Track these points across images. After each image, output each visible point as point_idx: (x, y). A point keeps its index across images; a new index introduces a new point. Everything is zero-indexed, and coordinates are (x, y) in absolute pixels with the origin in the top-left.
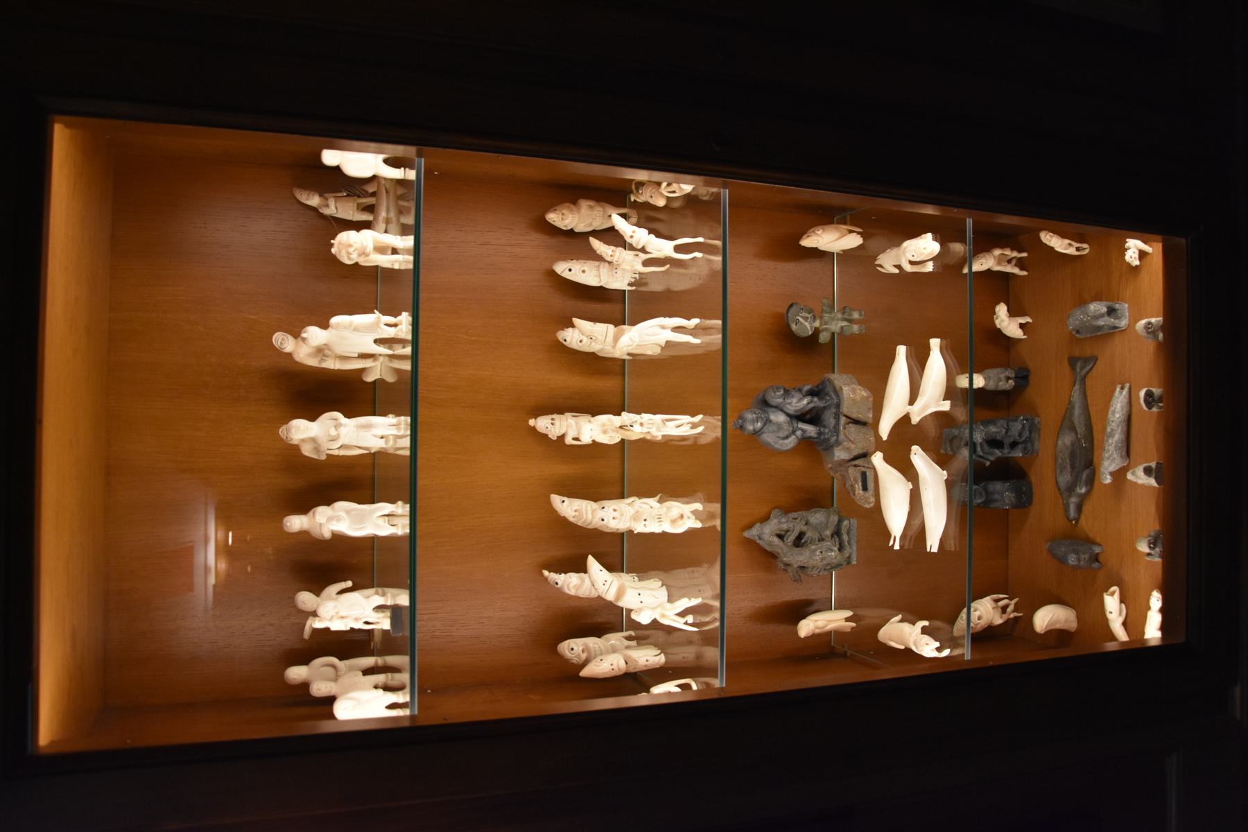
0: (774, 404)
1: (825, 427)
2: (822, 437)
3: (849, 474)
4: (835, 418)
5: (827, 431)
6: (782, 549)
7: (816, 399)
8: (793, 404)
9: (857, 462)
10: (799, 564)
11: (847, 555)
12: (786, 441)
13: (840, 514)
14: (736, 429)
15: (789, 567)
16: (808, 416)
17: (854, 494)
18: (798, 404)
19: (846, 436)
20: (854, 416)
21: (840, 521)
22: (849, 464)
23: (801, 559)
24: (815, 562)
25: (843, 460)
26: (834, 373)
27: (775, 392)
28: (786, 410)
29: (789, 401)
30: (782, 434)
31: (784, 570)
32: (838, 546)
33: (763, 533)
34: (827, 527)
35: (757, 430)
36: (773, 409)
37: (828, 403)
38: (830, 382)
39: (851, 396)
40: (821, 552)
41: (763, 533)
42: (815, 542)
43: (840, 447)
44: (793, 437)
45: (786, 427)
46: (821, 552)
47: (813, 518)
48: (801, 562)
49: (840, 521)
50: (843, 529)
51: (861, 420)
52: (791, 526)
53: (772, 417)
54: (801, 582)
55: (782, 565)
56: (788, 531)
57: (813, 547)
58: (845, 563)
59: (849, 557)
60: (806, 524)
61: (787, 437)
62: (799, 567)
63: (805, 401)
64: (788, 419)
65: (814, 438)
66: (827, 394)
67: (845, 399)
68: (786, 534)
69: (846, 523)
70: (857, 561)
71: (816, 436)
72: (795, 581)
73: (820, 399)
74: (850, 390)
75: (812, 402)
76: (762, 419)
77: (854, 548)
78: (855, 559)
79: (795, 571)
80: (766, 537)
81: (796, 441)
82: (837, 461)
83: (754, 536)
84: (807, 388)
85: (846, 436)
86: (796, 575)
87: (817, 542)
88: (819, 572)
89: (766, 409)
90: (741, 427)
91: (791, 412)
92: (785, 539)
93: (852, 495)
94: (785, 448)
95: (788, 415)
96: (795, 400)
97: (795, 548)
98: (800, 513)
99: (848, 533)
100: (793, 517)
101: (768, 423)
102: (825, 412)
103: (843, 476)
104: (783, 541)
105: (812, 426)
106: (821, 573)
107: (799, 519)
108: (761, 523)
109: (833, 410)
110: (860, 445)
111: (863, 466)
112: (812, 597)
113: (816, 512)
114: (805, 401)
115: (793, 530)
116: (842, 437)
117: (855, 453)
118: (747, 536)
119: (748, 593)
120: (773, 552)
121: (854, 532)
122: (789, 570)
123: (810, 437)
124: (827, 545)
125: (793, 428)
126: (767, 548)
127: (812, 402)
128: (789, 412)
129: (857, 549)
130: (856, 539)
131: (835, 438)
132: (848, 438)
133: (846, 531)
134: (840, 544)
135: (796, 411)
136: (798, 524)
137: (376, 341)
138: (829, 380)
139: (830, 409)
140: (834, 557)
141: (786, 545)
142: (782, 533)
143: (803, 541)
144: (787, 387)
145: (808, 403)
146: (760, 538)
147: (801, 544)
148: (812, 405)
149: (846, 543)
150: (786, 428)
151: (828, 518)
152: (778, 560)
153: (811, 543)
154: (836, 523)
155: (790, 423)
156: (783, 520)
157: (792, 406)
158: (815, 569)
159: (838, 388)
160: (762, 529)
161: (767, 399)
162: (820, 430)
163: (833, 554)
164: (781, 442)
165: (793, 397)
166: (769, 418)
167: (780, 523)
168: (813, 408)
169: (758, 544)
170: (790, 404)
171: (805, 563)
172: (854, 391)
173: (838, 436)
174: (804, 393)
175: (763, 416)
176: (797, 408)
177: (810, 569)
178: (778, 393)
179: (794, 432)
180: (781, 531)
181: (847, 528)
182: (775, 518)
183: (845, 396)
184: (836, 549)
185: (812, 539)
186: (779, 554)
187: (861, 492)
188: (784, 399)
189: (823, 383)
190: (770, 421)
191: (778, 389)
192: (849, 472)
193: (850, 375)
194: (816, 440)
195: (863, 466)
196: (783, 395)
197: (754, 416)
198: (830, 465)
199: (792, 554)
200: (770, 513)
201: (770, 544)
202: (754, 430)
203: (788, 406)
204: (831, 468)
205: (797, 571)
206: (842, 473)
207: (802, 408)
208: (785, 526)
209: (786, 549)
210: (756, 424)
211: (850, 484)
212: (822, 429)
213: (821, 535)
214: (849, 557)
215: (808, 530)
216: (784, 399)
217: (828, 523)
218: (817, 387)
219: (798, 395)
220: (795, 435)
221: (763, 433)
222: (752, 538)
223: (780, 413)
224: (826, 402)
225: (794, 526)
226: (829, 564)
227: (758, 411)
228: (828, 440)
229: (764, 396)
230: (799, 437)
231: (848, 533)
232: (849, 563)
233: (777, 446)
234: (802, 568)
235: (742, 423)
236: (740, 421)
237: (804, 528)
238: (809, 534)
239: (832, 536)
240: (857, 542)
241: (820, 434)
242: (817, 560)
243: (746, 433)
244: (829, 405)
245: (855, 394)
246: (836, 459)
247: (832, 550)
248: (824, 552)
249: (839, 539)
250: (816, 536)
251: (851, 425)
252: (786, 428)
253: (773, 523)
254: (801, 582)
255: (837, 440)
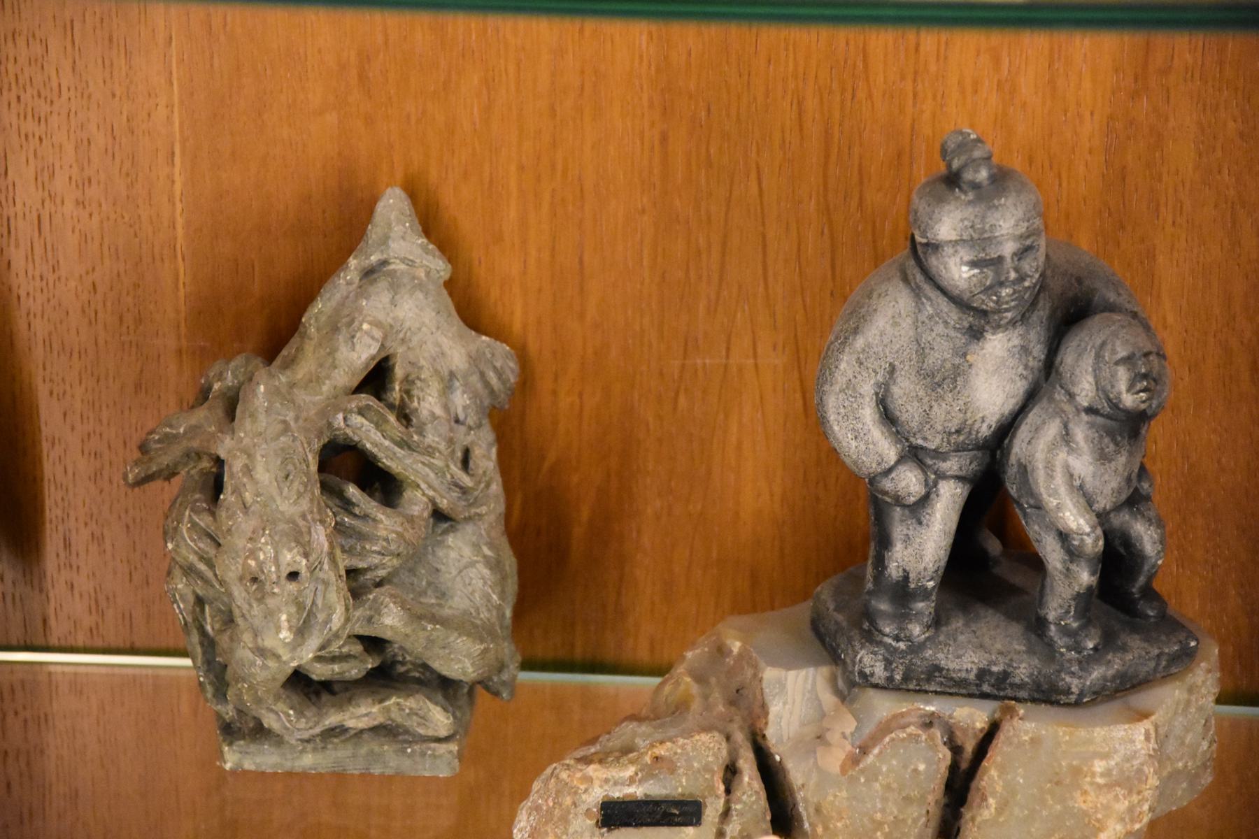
0: (1068, 357)
1: (937, 622)
2: (884, 606)
3: (688, 734)
4: (983, 674)
5: (916, 630)
6: (314, 381)
7: (1085, 577)
8: (1062, 455)
9: (749, 776)
10: (236, 466)
11: (269, 721)
12: (869, 413)
13: (482, 695)
14: (944, 151)
15: (220, 412)
16: (993, 546)
17: (586, 760)
18: (1059, 480)
19: (885, 728)
20: (992, 776)
21: (445, 687)
22: (740, 737)
23: (263, 475)
24: (241, 543)
25: (764, 707)
26: (1219, 701)
27: (1128, 360)
28: (1033, 417)
29: (1080, 433)
30: (905, 392)
31: (204, 395)
32: (320, 672)
33: (395, 287)
34: (418, 617)
35: (933, 262)
36: (1039, 351)
37: (1061, 642)
38: (1175, 659)
39: (1099, 766)
40: (293, 576)
41: (395, 287)
42: (348, 551)
43: (828, 699)
44: (890, 452)
45: (945, 415)
46: (293, 576)
47: (467, 552)
48: (248, 470)
49: (445, 687)
50: (411, 703)
51: (967, 814)
52: (431, 438)
53: (997, 345)
54: (140, 482)
55: (230, 379)
56: (405, 417)
57: (320, 536)
58: (229, 712)
59: (259, 732)
60: (439, 515)
61: (888, 417)
62: (219, 462)
63: (1076, 520)
64: (985, 431)
65: (880, 563)
66: (1109, 642)
67: (1082, 733)
68: (391, 407)
69: (439, 719)
70: (238, 773)
71: (893, 571)
72: (143, 448)
73: (1086, 603)
74: (1128, 759)
75: (1073, 553)
76: (988, 290)
77: (308, 761)
78: (248, 765)
79: (195, 444)
80: (377, 304)
81: (870, 464)
82: (757, 678)
83: (385, 240)
84: (1146, 536)
85: (885, 728)
86: (176, 452)
87: (344, 562)
88: (189, 571)
89: (1042, 313)
90: (952, 180)
91: (1019, 447)
92: (366, 399)
93: (580, 753)
94: (833, 405)
95: (1007, 429)
96: (1083, 465)
97: (317, 445)
98: (496, 488)
99: (386, 731)
100: (477, 452)
101: (968, 320)
102: (1016, 629)
103: (680, 708)
104: (359, 389)
105: (943, 555)
106: (181, 585)
107: (467, 481)
108: (450, 285)
109: (1023, 671)
110: (837, 797)
111: (726, 814)
112: (52, 544)
113: (495, 565)
114: (1076, 520)
115: (403, 444)
116: (884, 706)
117: (797, 774)
118: (380, 207)
119: (80, 203)
120: (295, 341)
121: (391, 760)
122: (201, 414)
123: (885, 542)
124: (330, 610)
125: (938, 454)
126: (321, 308)
127: (1073, 553)
128: (1023, 433)
129: (304, 776)
130: (354, 768)
131: (879, 671)
132: (875, 739)
133: (396, 716)
134: (327, 686)
135: (1024, 470)
136: (440, 473)
137: (66, 58)
138: (1185, 657)
139: (1030, 651)
140: (268, 642)
141: (332, 405)
142: (395, 394)
143: (352, 491)
144: (1155, 431)
145: (1064, 537)
146: (369, 274)
147: (333, 479)
148: (1053, 554)
149: (333, 719)
150: (939, 412)
151: (465, 625)
152: (258, 361)
153: (339, 529)
154: (436, 665)
155: (961, 440)
156: (460, 400)
157: (1053, 447)
158: (205, 545)
159: (1142, 699)
160: (421, 286)
161: (1095, 321)
162: (925, 594)
163: (285, 635)
164: (868, 389)
165: (1102, 457)
166: (997, 328)
167: (448, 381)
168: (1037, 564)
169: (337, 263)
170: (1066, 437)
171: (237, 491)
172: (1126, 781)
173: (889, 686)
174: (1117, 520)
175: (1005, 292)
176: (1040, 476)
177: (204, 521)
178: (1123, 375)
179: (914, 455)
180: (407, 380)
181: (412, 723)
182: (475, 360)
183: (1099, 732)
184: (306, 655)
185: (362, 537)
186: (289, 364)
187: (596, 795)
188: (1090, 410)
189: (1169, 624)
190: (976, 334)
191: (1148, 380)
192: (705, 737)
193: (1207, 779)
194: (869, 571)
195: (726, 814)
196: (1115, 405)
197: (1008, 249)
198: (736, 646)
199: (286, 429)
200: (498, 333)
201: (339, 325)
202: (935, 247)
203: (1053, 429)
204: (721, 651)
205: (199, 455)
206: (696, 706)
207: (1039, 507)
208: (428, 403)
209: (311, 400)
210: (966, 254)
211: (639, 742)
212: (923, 607)
213: (379, 584)
214: (259, 732)
215: (411, 520)
216: (1090, 410)
217: (444, 622)
218: (1149, 593)
219: (1108, 486)
220: (901, 460)
221: (917, 293)
222: (374, 232)
223: (1020, 387)
224: (1066, 631)
225: (430, 451)
226: (229, 620)
227: (1031, 266)
228: (871, 637)
229: (1111, 308)
230: (887, 484)
231: (386, 731)
232: (229, 731)
233: (845, 366)
234: (214, 486)
235: (976, 186)
236: (983, 174)
237: (416, 503)
238: (386, 523)
239: (373, 644)
240: (339, 777)
241: (903, 593)
242: (253, 554)
243: (921, 205)
244: (1050, 645)
245: (1109, 787)
246: (770, 674)
247: (301, 632)
248: (292, 587)
249: (357, 683)
250: (377, 560)
251: (945, 755)
252: (939, 412)
253: (446, 342)
254: (140, 482)
255: (866, 681)
